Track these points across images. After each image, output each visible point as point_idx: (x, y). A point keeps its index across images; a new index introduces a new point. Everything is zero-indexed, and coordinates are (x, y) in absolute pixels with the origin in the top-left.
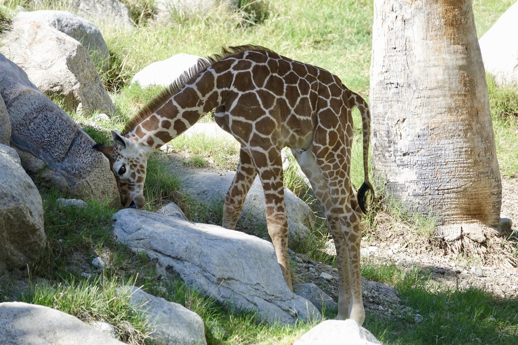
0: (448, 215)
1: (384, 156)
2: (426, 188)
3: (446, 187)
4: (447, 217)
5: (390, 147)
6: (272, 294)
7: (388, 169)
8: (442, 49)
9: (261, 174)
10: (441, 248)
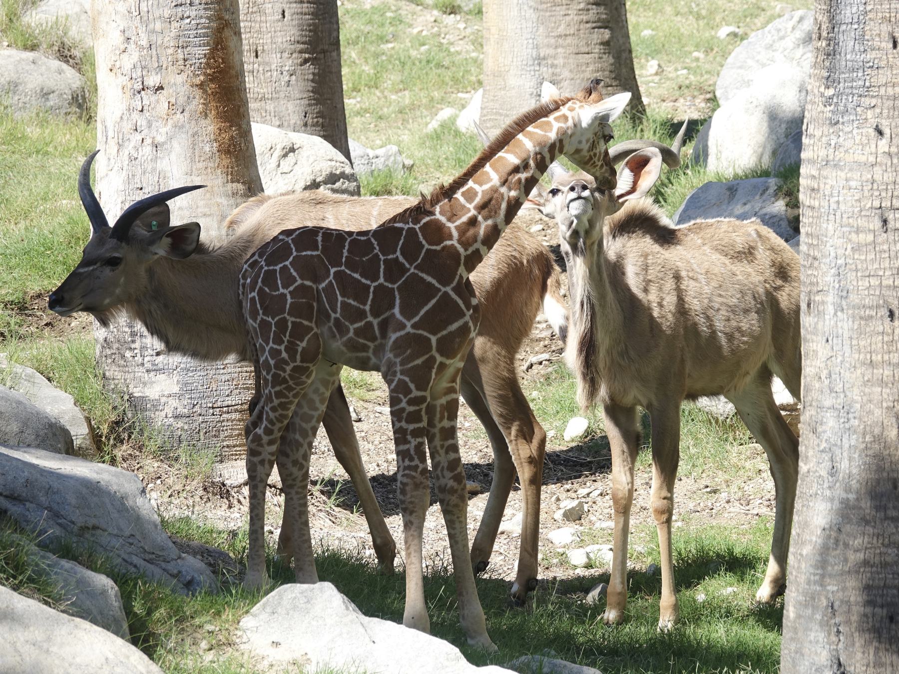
0: (228, 446)
1: (123, 356)
2: (194, 405)
3: (226, 403)
4: (226, 449)
5: (133, 342)
6: (152, 551)
7: (128, 376)
8: (216, 188)
9: (464, 351)
10: (222, 498)
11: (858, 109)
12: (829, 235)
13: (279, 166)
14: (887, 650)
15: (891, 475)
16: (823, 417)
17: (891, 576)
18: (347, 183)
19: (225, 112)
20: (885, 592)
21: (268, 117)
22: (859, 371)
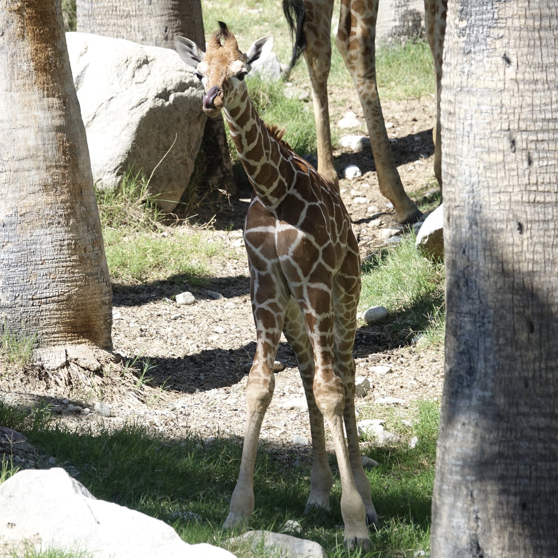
0: (47, 334)
2: (16, 297)
3: (44, 295)
4: (45, 336)
8: (33, 103)
10: (41, 379)
11: (488, 39)
12: (464, 155)
13: (134, 76)
14: (520, 535)
15: (522, 374)
16: (461, 321)
17: (523, 467)
18: (195, 91)
19: (41, 35)
20: (518, 481)
21: (133, 32)
22: (492, 280)
